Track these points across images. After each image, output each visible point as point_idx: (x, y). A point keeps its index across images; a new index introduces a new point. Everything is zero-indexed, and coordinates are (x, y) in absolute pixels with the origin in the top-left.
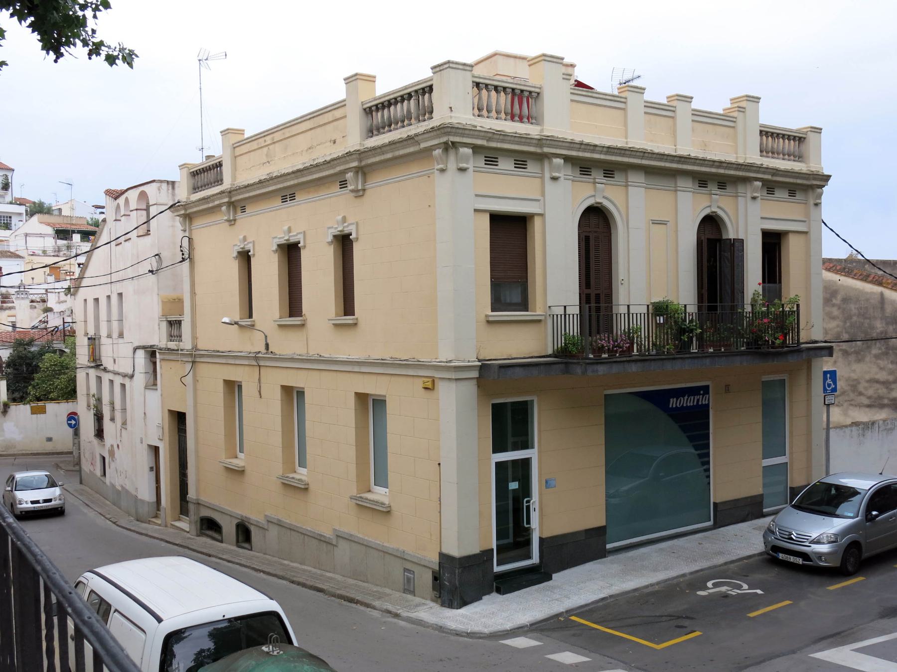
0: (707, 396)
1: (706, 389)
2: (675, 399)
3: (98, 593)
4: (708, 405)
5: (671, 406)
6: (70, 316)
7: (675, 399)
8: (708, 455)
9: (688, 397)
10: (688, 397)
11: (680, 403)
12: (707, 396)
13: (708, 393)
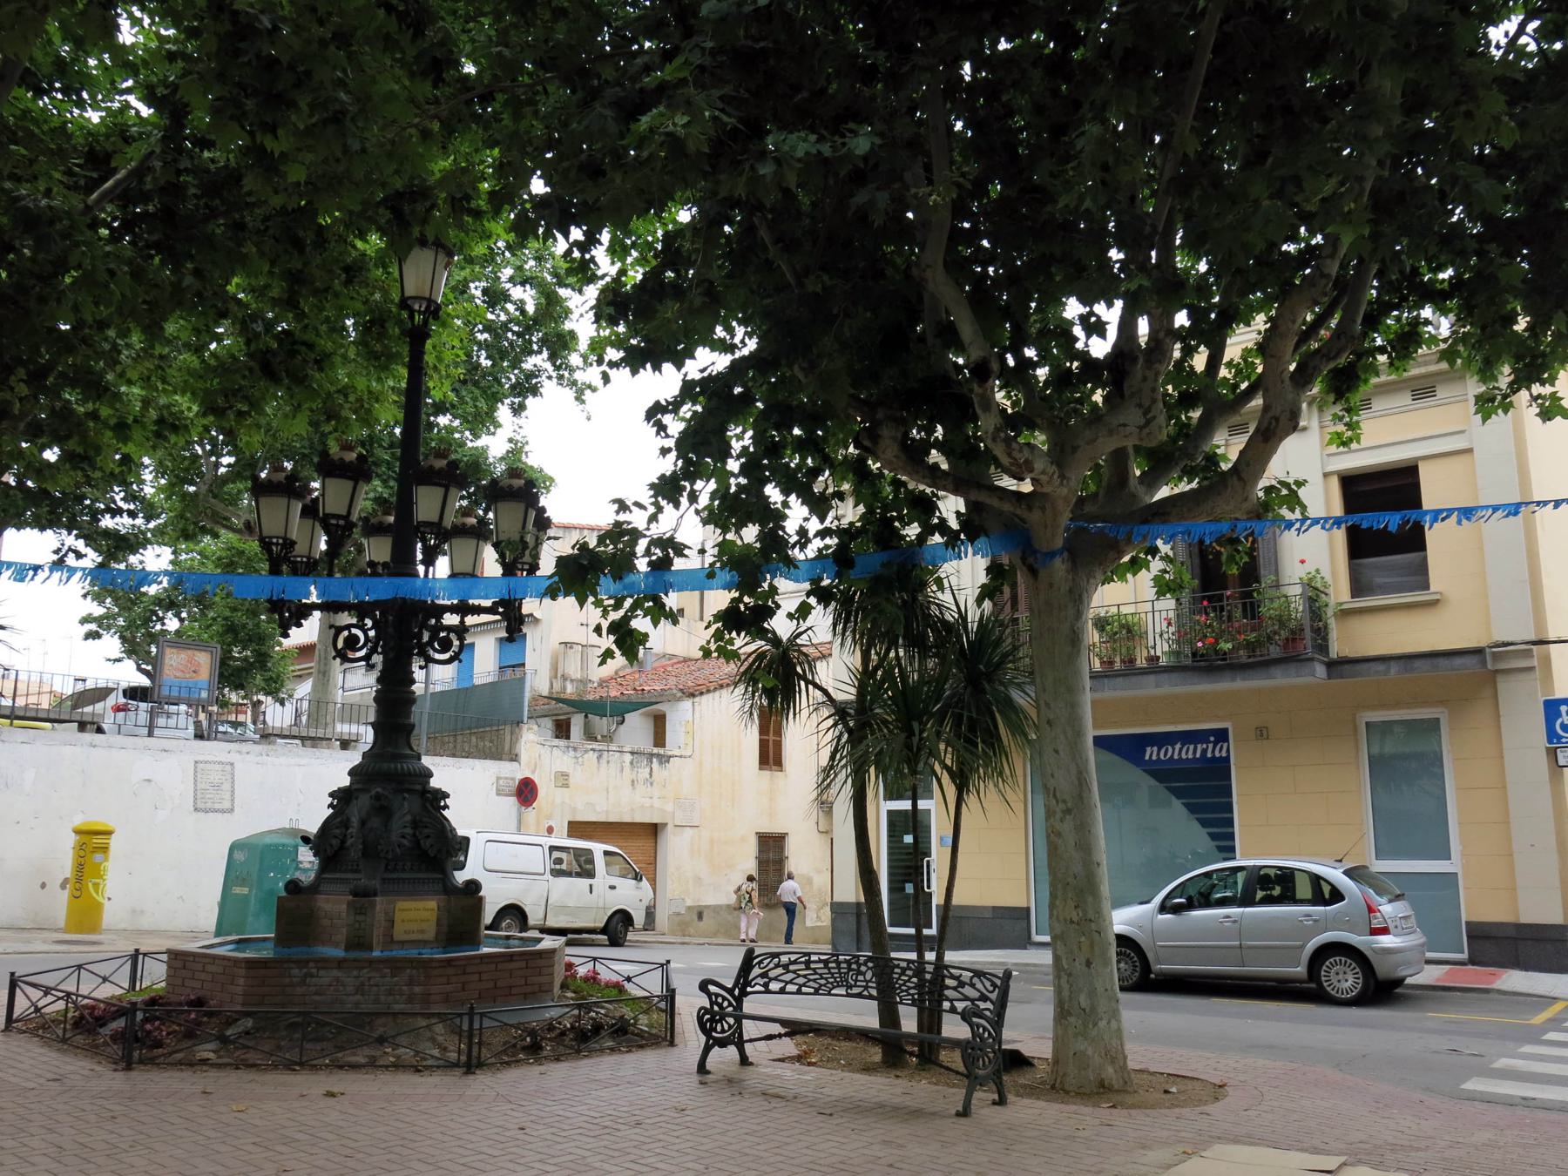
0: (1225, 745)
1: (1221, 736)
2: (1155, 749)
3: (613, 818)
4: (1227, 759)
5: (1147, 758)
6: (659, 722)
7: (1155, 749)
8: (1231, 837)
9: (1183, 745)
10: (1183, 745)
11: (1166, 754)
12: (1225, 745)
13: (1227, 740)
